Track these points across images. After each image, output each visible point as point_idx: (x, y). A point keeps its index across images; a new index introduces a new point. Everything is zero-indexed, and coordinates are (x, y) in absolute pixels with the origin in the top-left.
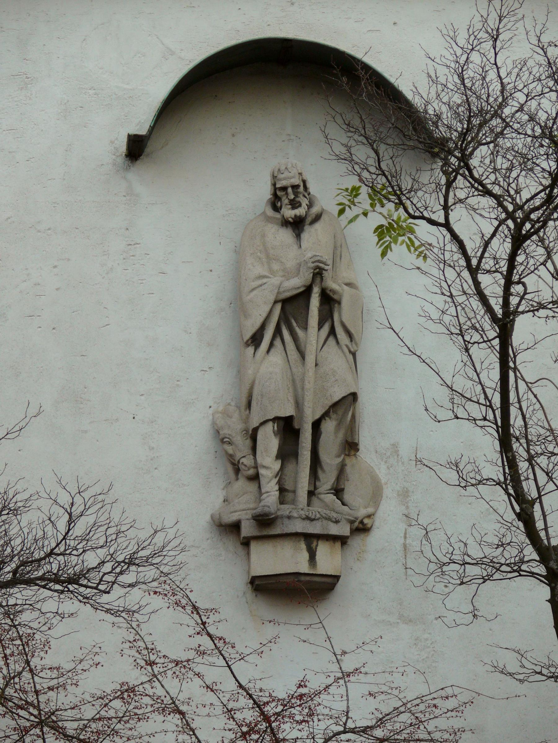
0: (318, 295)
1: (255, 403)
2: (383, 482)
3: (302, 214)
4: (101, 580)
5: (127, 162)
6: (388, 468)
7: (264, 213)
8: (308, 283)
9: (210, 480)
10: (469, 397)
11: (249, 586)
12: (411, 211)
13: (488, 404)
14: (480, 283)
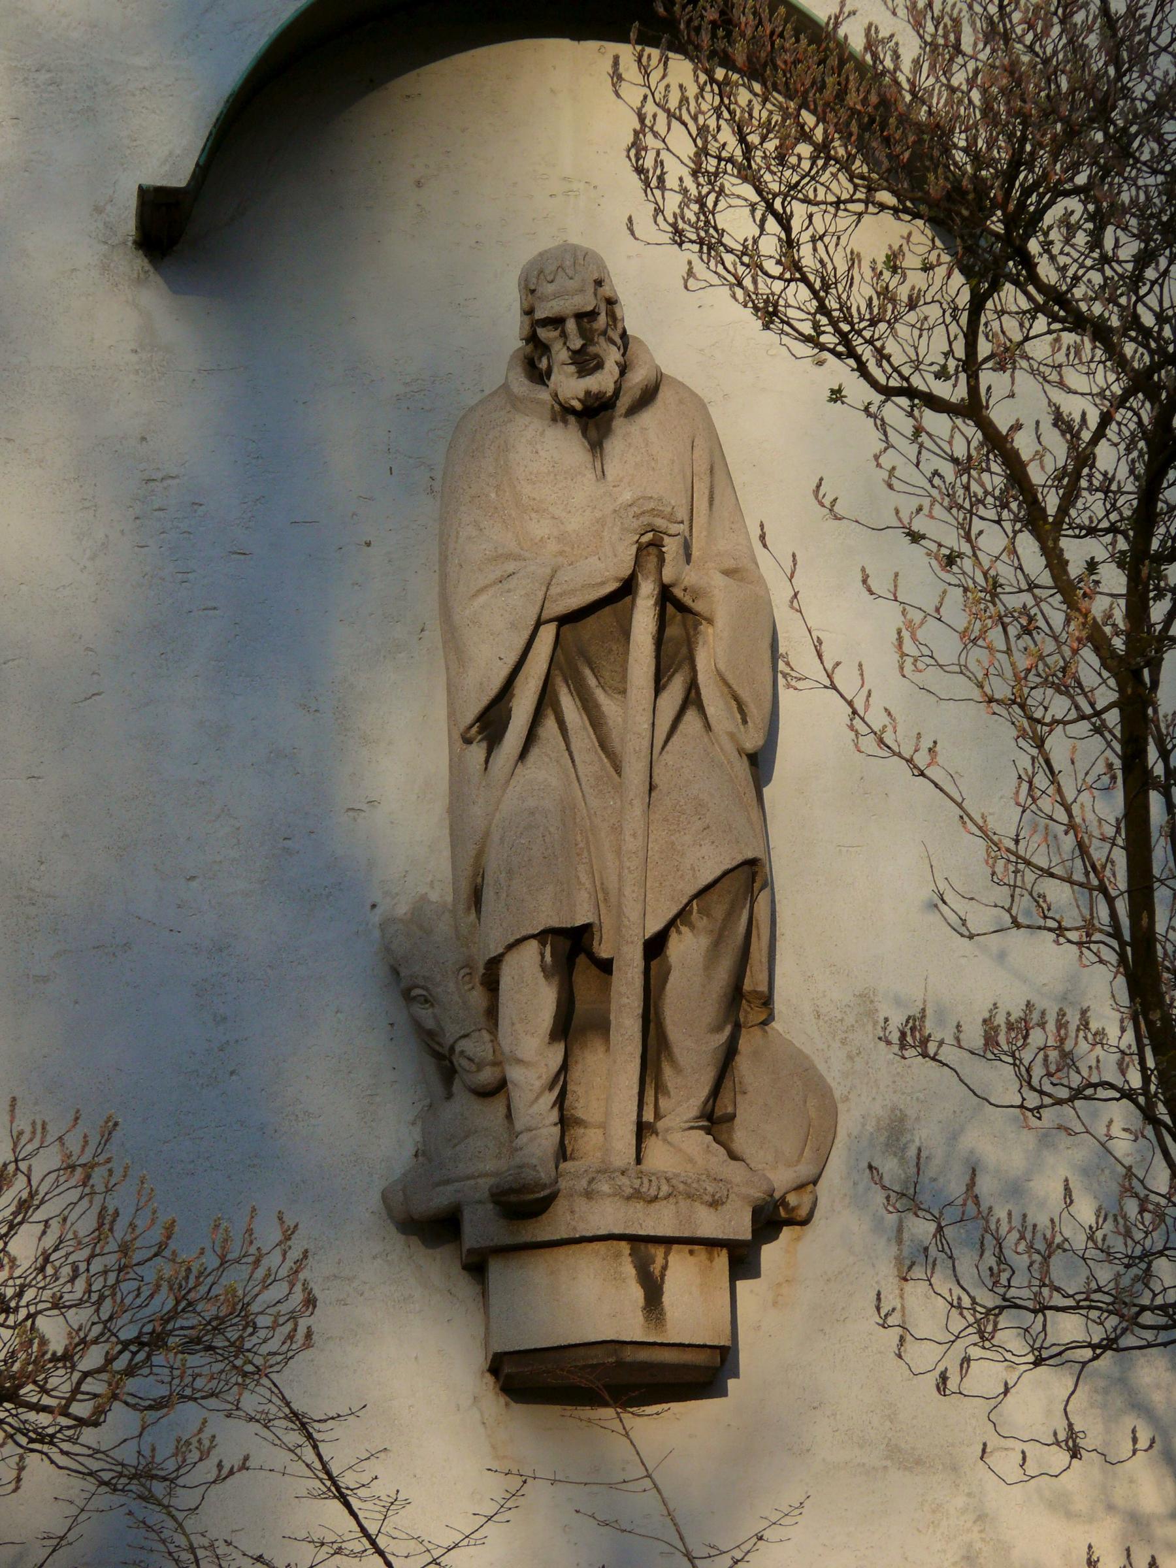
0: (652, 602)
1: (492, 894)
2: (837, 1094)
3: (603, 389)
4: (76, 1390)
5: (139, 261)
6: (850, 1057)
7: (505, 387)
8: (626, 572)
9: (378, 1099)
10: (1045, 866)
11: (489, 1379)
12: (882, 380)
13: (1095, 882)
14: (1067, 562)
